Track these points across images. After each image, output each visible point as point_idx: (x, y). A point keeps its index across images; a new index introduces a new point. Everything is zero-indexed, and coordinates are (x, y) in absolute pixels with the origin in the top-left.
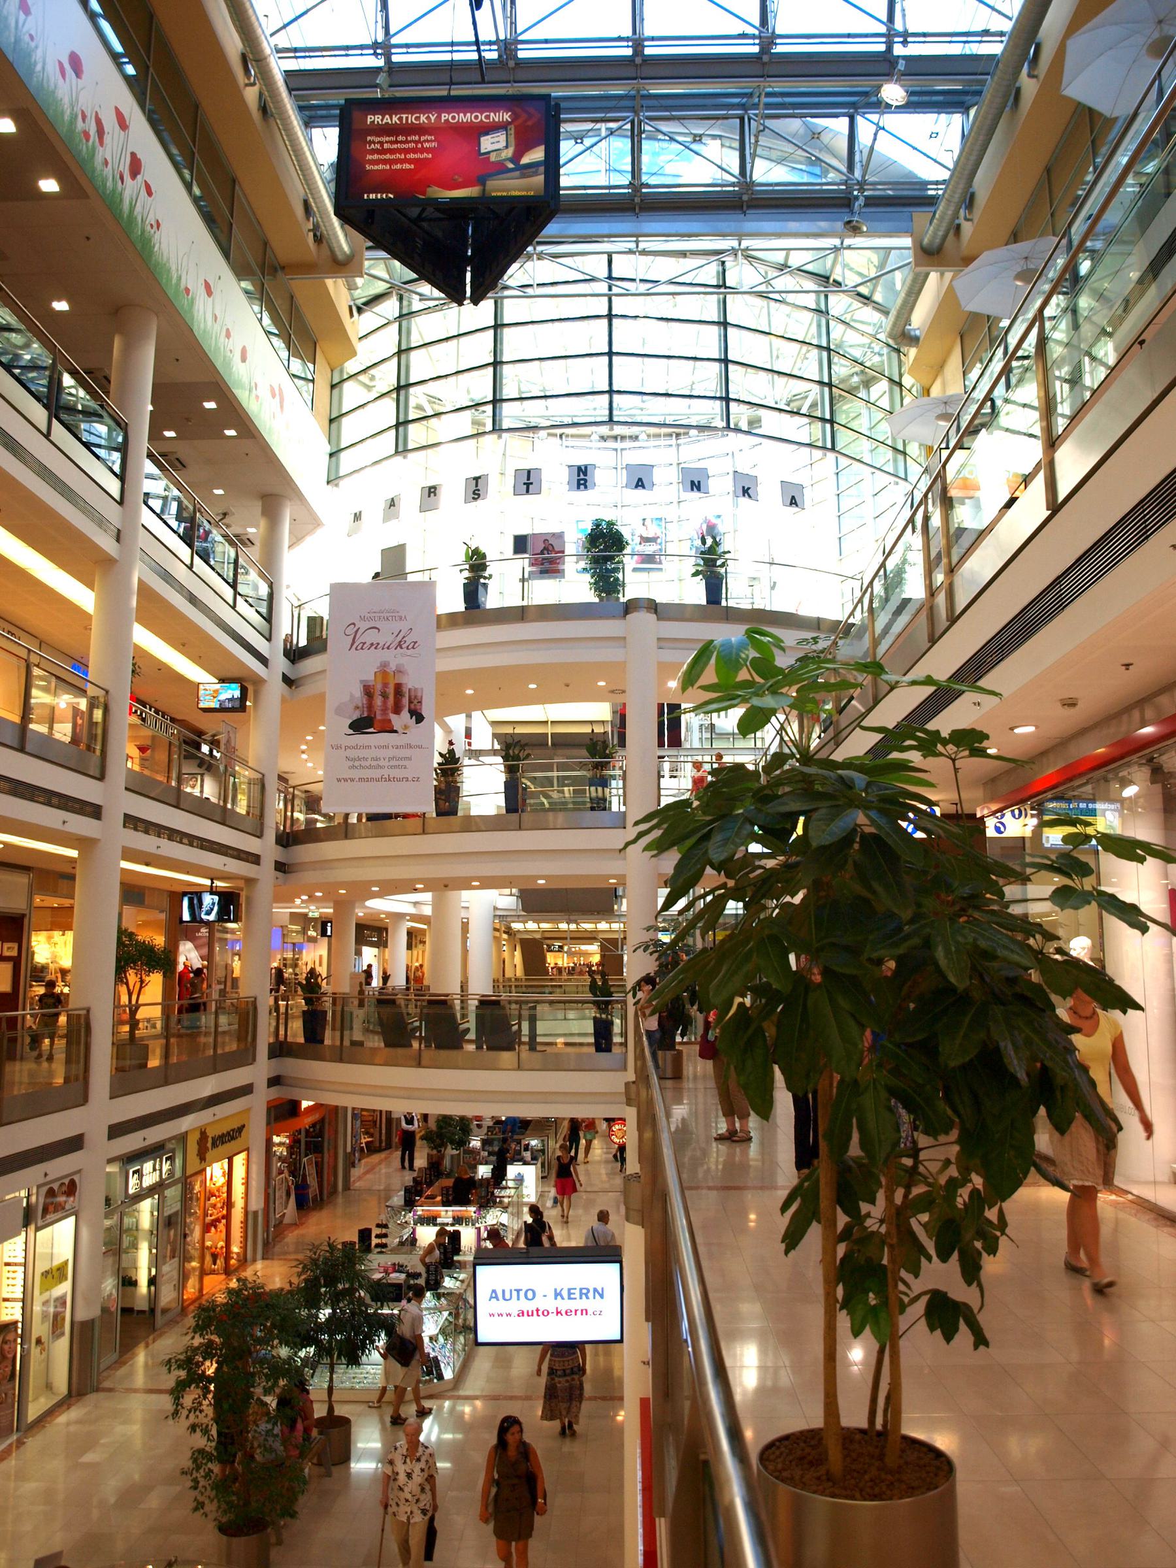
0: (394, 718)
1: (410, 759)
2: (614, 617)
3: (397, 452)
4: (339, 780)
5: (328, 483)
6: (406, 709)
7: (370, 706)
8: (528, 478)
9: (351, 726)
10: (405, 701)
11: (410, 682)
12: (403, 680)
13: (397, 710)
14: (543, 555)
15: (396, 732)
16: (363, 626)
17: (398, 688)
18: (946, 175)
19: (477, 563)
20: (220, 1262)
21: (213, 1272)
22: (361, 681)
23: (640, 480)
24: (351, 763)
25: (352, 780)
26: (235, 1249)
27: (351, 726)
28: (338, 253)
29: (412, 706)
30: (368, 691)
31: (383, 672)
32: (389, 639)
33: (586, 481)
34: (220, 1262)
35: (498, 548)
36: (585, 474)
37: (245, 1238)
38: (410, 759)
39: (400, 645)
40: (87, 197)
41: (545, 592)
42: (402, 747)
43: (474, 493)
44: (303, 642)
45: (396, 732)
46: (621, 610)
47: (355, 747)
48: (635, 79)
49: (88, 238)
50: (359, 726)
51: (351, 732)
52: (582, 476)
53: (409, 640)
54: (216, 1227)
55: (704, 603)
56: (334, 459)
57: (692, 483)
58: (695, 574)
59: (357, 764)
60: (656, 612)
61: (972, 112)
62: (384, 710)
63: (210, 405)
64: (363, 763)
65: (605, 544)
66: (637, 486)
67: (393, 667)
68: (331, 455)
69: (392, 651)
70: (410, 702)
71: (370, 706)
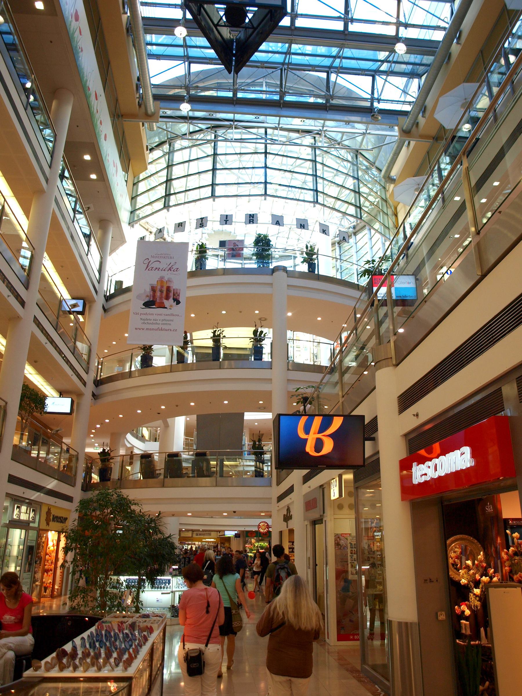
0: (165, 301)
1: (172, 321)
2: (267, 274)
3: (165, 207)
4: (136, 329)
5: (129, 224)
6: (172, 298)
7: (154, 296)
8: (227, 218)
9: (144, 304)
10: (171, 294)
11: (174, 286)
12: (171, 285)
13: (167, 298)
14: (233, 249)
15: (166, 308)
16: (153, 260)
17: (168, 289)
18: (414, 100)
19: (202, 250)
20: (49, 591)
21: (44, 597)
22: (150, 284)
23: (278, 221)
24: (143, 321)
25: (143, 329)
26: (56, 587)
27: (144, 304)
28: (149, 109)
29: (175, 297)
30: (153, 289)
31: (161, 281)
32: (165, 266)
33: (253, 220)
34: (49, 591)
35: (212, 244)
36: (253, 217)
37: (62, 581)
38: (172, 321)
39: (170, 269)
40: (56, 15)
41: (233, 264)
42: (168, 315)
43: (200, 224)
44: (112, 291)
45: (166, 308)
46: (270, 272)
47: (146, 314)
48: (291, 35)
49: (51, 42)
50: (148, 304)
51: (144, 307)
52: (251, 218)
53: (174, 267)
54: (47, 573)
55: (307, 271)
56: (132, 214)
57: (301, 225)
58: (303, 262)
59: (146, 322)
60: (287, 273)
61: (424, 78)
62: (161, 298)
63: (87, 157)
64: (149, 322)
65: (263, 244)
66: (276, 224)
67: (166, 279)
68: (131, 212)
69: (166, 272)
70: (174, 295)
71: (154, 296)
